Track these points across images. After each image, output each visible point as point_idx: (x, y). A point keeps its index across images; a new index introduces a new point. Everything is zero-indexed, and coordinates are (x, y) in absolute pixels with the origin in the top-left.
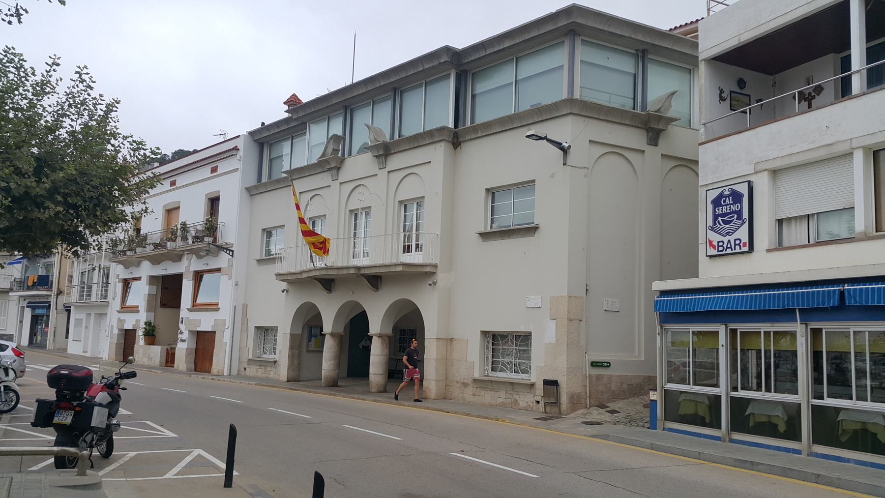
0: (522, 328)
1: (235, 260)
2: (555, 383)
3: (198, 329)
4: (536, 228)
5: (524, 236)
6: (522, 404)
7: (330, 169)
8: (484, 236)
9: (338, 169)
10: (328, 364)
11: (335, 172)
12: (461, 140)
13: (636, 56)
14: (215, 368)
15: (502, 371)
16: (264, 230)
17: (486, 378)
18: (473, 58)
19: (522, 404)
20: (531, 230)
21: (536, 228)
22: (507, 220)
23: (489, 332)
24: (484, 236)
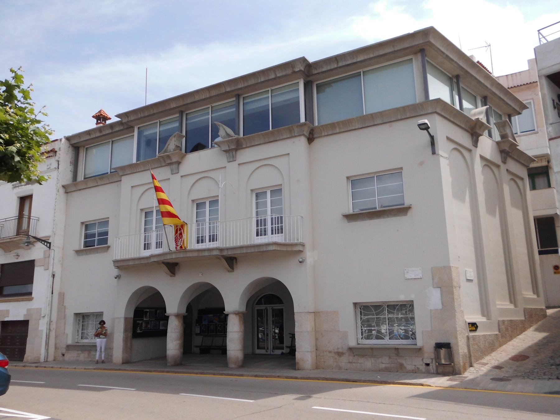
0: (402, 297)
1: (52, 252)
2: (447, 346)
3: (6, 319)
4: (409, 208)
5: (87, 254)
6: (409, 367)
7: (170, 164)
8: (350, 217)
9: (179, 163)
10: (173, 343)
11: (174, 166)
12: (315, 136)
13: (450, 79)
14: (29, 354)
15: (87, 338)
16: (82, 223)
17: (77, 344)
18: (324, 70)
19: (409, 367)
20: (403, 210)
21: (409, 208)
22: (377, 202)
23: (79, 314)
24: (350, 217)
